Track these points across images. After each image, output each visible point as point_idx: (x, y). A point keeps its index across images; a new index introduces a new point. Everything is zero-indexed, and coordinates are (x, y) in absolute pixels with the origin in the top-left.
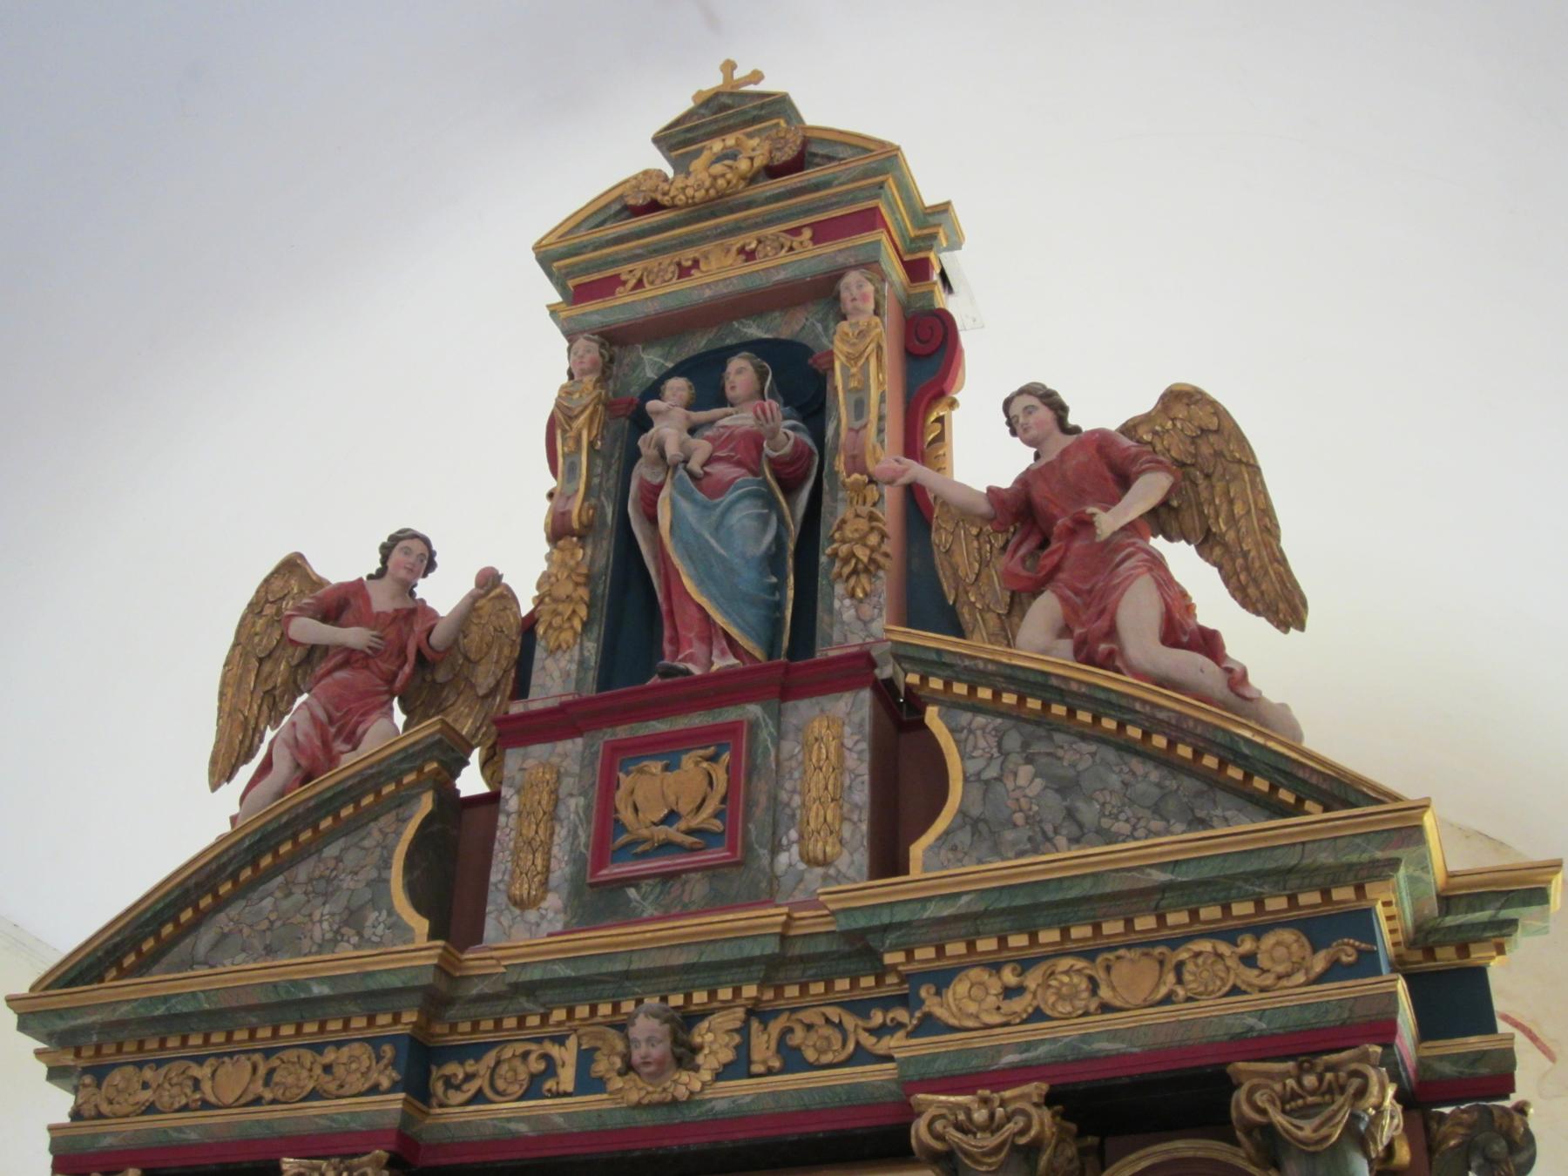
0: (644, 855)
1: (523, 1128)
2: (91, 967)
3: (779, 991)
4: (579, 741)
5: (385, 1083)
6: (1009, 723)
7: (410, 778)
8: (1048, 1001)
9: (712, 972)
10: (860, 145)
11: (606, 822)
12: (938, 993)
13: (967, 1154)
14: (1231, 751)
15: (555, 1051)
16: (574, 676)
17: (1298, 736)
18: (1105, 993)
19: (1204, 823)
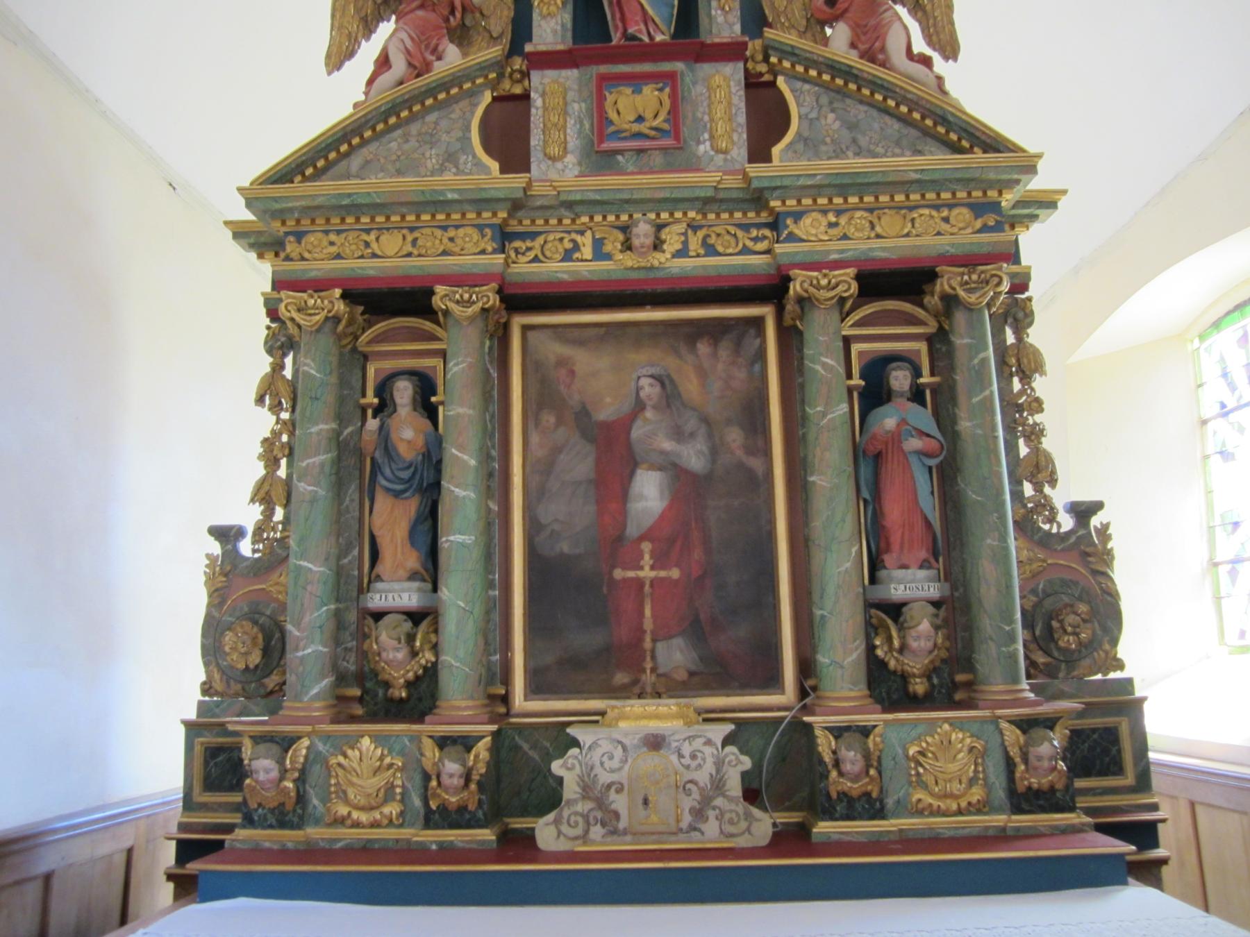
0: (625, 139)
1: (565, 277)
2: (286, 175)
3: (705, 215)
4: (575, 71)
5: (490, 249)
6: (822, 90)
8: (851, 231)
9: (673, 203)
11: (602, 120)
12: (796, 222)
13: (817, 300)
15: (579, 238)
16: (560, 33)
18: (878, 229)
19: (920, 153)
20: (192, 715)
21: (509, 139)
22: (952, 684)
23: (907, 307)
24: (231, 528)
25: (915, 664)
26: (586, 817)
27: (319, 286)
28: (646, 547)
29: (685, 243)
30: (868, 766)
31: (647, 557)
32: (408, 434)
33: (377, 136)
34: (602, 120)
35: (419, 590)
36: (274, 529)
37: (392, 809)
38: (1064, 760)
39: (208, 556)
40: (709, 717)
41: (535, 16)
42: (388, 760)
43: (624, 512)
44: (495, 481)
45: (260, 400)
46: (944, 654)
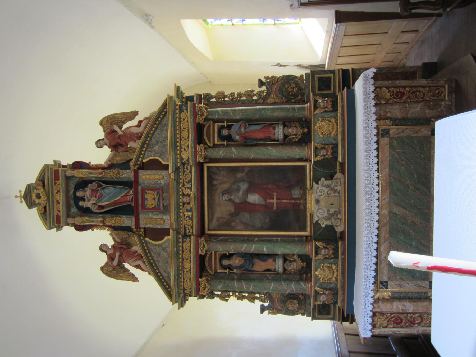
3: (181, 183)
5: (189, 240)
7: (143, 241)
8: (186, 145)
9: (178, 191)
10: (43, 171)
11: (154, 209)
14: (157, 119)
15: (186, 216)
17: (155, 112)
18: (186, 138)
20: (310, 318)
22: (305, 123)
23: (205, 129)
24: (261, 308)
25: (300, 131)
26: (335, 219)
27: (198, 284)
28: (268, 201)
29: (188, 188)
30: (324, 148)
31: (271, 201)
32: (237, 261)
33: (158, 269)
34: (154, 209)
35: (278, 259)
36: (261, 297)
37: (334, 267)
38: (325, 98)
39: (268, 314)
40: (312, 187)
41: (124, 225)
42: (321, 268)
43: (259, 205)
44: (249, 239)
45: (227, 300)
46: (297, 124)
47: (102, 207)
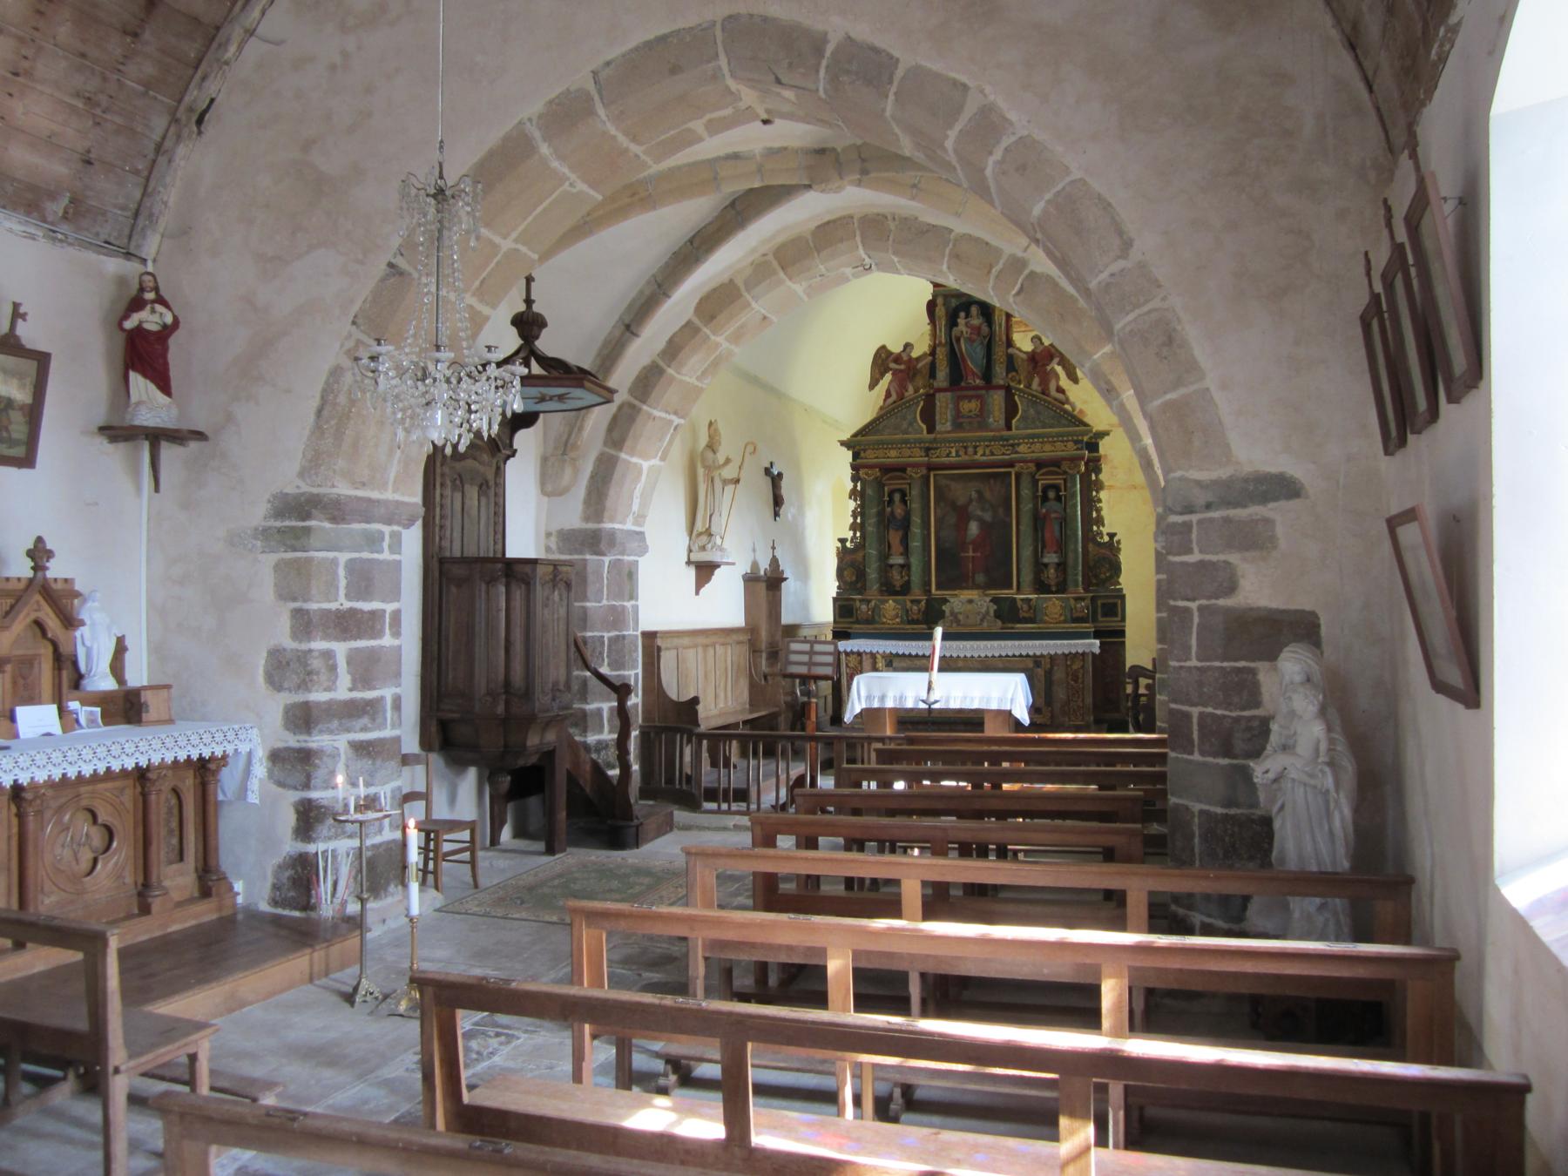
21: (929, 417)
22: (1062, 588)
47: (958, 340)
